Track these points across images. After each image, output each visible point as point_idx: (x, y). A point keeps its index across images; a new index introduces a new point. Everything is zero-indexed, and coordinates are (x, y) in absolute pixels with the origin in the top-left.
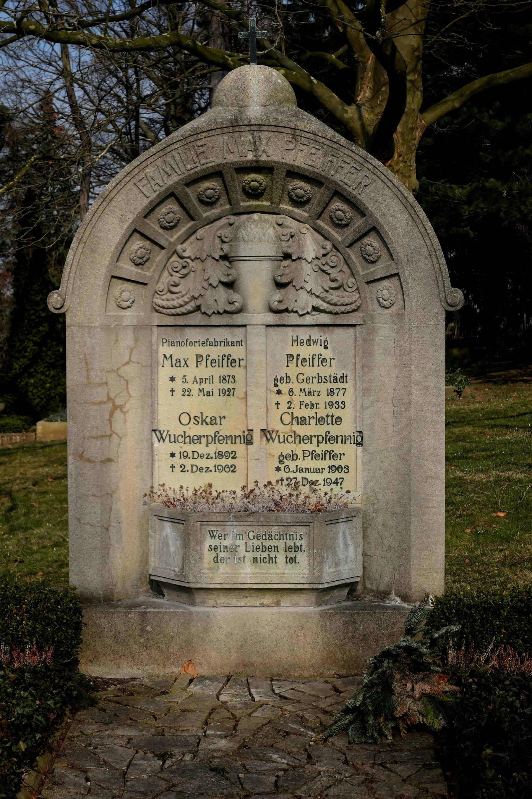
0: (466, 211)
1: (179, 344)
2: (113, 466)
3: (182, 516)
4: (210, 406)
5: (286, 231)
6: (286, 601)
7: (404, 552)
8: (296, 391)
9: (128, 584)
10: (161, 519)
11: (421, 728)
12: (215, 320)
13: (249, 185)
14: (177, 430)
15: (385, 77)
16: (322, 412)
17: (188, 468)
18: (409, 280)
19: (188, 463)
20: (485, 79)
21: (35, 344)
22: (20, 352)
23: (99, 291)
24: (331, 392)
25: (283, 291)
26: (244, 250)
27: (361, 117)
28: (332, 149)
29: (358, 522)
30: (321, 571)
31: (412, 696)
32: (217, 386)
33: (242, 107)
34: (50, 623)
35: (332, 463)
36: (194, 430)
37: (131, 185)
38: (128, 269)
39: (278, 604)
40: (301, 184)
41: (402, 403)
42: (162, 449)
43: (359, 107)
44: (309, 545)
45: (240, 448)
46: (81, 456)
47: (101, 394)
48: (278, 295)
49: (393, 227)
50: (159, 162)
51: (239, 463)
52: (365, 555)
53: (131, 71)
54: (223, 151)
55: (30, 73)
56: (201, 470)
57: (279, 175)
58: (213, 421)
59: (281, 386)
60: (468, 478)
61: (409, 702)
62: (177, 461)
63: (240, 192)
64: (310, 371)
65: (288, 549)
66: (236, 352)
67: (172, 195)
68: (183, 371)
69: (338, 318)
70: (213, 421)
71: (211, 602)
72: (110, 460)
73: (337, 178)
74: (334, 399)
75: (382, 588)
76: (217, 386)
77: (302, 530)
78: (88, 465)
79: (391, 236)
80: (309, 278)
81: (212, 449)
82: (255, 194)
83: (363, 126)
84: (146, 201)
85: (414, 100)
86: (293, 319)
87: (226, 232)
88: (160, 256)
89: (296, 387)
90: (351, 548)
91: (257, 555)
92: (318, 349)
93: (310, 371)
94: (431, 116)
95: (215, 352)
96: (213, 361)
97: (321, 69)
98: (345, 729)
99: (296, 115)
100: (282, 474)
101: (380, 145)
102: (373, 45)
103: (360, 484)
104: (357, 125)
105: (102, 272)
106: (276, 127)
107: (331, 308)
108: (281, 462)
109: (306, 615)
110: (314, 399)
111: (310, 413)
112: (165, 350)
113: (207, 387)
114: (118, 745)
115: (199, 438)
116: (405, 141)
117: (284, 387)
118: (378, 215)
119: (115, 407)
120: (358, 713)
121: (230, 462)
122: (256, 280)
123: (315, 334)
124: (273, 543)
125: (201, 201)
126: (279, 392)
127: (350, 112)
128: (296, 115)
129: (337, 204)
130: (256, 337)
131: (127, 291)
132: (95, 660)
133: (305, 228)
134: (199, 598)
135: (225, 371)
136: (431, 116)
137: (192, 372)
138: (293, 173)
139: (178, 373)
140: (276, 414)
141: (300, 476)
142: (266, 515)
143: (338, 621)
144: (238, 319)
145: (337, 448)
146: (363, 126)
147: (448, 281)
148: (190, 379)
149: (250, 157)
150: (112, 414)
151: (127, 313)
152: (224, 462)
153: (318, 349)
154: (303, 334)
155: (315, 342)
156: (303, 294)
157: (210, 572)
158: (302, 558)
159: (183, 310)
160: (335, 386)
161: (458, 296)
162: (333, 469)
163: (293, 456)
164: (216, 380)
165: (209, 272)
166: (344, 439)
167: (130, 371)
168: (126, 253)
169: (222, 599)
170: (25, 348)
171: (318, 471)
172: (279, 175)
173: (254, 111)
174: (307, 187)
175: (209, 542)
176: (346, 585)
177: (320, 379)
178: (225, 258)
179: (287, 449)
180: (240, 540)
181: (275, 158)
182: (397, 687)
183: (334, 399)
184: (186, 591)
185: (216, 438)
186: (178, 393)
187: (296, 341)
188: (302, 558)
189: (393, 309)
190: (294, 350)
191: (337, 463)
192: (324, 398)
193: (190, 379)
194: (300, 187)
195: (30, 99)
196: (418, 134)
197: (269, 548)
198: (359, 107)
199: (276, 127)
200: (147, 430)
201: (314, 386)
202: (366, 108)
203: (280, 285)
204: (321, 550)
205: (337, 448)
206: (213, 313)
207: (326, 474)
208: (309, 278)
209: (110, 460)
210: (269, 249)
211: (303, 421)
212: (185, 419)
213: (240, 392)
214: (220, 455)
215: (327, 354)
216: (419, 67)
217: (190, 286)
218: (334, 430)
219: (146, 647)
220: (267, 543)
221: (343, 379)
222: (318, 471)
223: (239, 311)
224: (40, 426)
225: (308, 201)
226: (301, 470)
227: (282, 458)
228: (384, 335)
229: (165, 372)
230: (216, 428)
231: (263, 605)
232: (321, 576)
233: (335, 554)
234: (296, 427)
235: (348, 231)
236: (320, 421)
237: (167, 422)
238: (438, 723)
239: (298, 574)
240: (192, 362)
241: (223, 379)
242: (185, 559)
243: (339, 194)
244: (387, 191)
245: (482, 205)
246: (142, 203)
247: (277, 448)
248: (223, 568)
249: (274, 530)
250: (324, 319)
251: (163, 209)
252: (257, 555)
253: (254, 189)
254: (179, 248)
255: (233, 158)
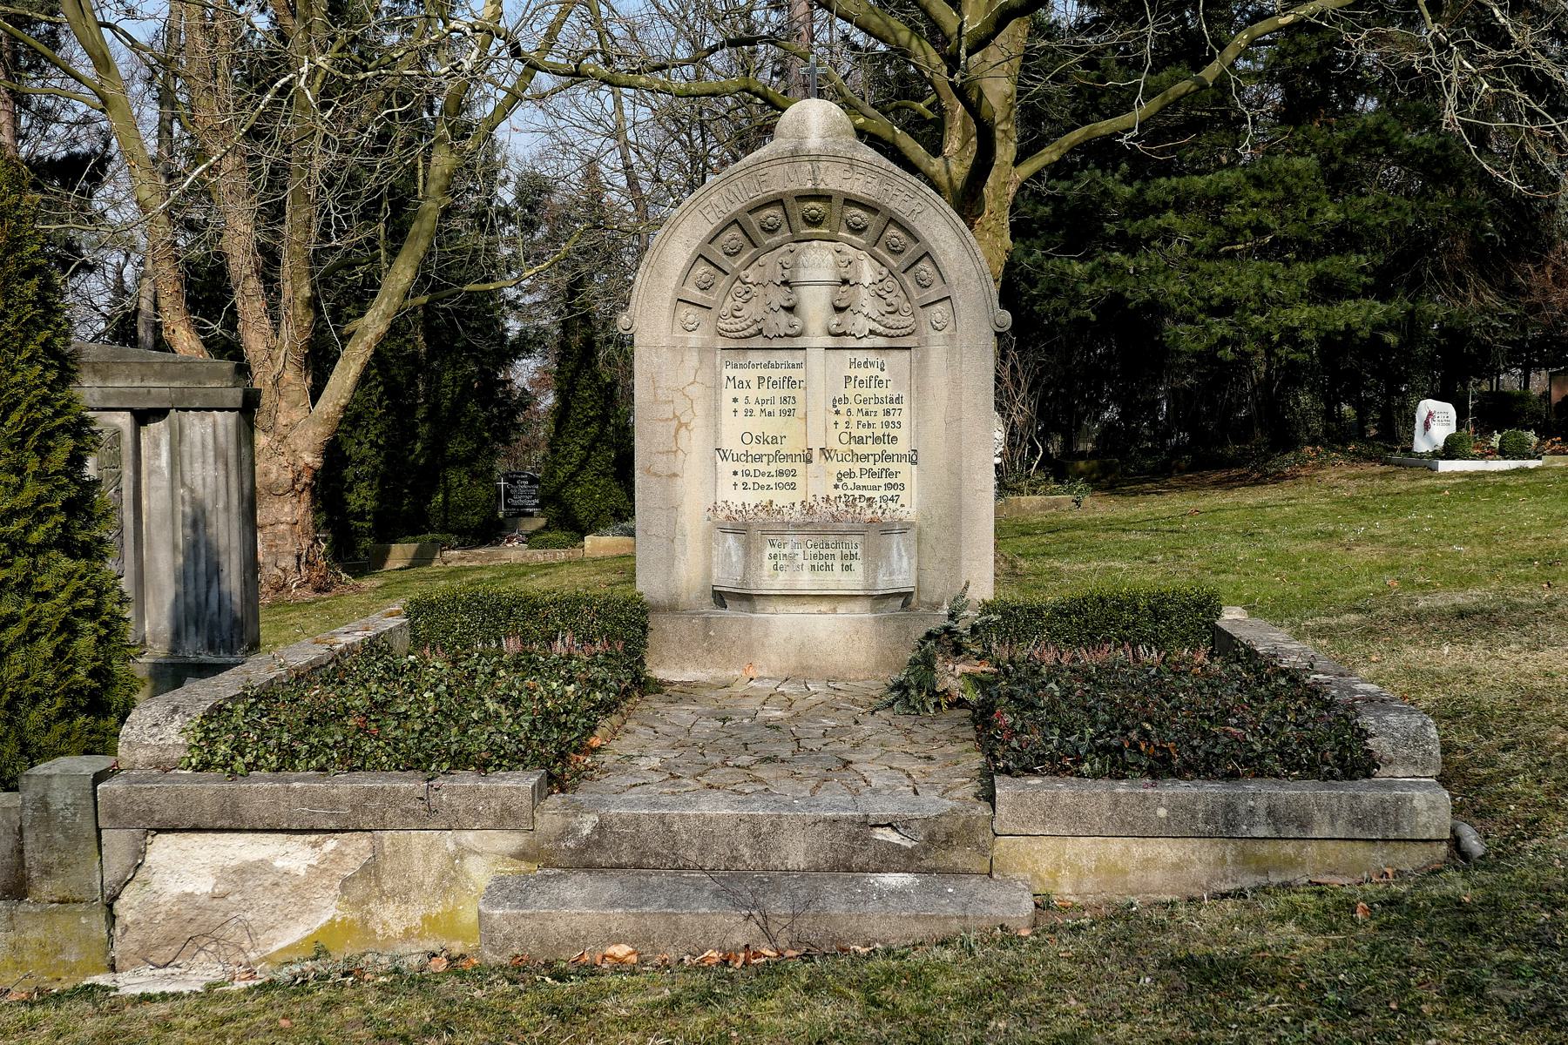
0: (1085, 289)
1: (742, 366)
2: (679, 481)
3: (744, 530)
4: (771, 426)
5: (844, 258)
6: (842, 608)
7: (955, 562)
8: (854, 411)
9: (693, 596)
10: (724, 531)
11: (960, 703)
12: (776, 343)
13: (809, 213)
14: (739, 449)
15: (973, 128)
16: (879, 432)
17: (750, 485)
18: (959, 302)
19: (750, 480)
20: (1086, 128)
21: (583, 448)
22: (564, 457)
23: (666, 313)
24: (887, 413)
25: (842, 315)
26: (804, 275)
27: (948, 171)
28: (886, 178)
29: (912, 534)
30: (875, 578)
31: (953, 676)
32: (777, 407)
33: (802, 139)
34: (619, 622)
35: (889, 480)
36: (756, 449)
37: (696, 212)
38: (694, 293)
39: (834, 611)
40: (859, 211)
41: (953, 420)
42: (726, 467)
43: (946, 159)
44: (864, 553)
45: (799, 466)
46: (648, 470)
47: (667, 411)
48: (836, 319)
49: (944, 253)
50: (723, 191)
51: (798, 480)
52: (919, 569)
53: (695, 134)
54: (782, 181)
55: (574, 135)
56: (762, 487)
57: (837, 203)
58: (775, 440)
59: (839, 407)
60: (1066, 568)
61: (950, 679)
62: (740, 479)
63: (800, 219)
64: (867, 392)
65: (844, 557)
66: (797, 374)
67: (736, 221)
68: (746, 392)
69: (894, 341)
70: (775, 440)
71: (771, 609)
72: (675, 475)
73: (892, 205)
74: (890, 419)
75: (935, 600)
76: (777, 407)
77: (857, 539)
78: (654, 479)
79: (942, 260)
80: (867, 302)
81: (773, 467)
82: (814, 222)
83: (950, 180)
84: (711, 227)
85: (1005, 152)
86: (850, 342)
87: (788, 259)
88: (723, 282)
89: (854, 408)
90: (905, 559)
91: (815, 563)
92: (875, 371)
93: (867, 392)
94: (1027, 169)
95: (776, 374)
96: (774, 383)
97: (900, 113)
98: (891, 705)
99: (854, 146)
100: (840, 492)
101: (968, 201)
102: (961, 92)
103: (915, 500)
104: (944, 180)
105: (669, 295)
106: (835, 157)
107: (887, 331)
108: (839, 479)
109: (861, 621)
110: (871, 419)
111: (868, 432)
112: (729, 372)
113: (768, 408)
114: (684, 715)
115: (761, 456)
116: (996, 197)
117: (842, 408)
118: (930, 240)
119: (681, 425)
120: (901, 687)
121: (790, 480)
122: (815, 303)
123: (872, 356)
124: (829, 552)
125: (763, 229)
126: (837, 412)
127: (936, 165)
128: (854, 146)
129: (893, 231)
130: (816, 358)
131: (691, 314)
132: (661, 663)
133: (862, 255)
134: (759, 605)
135: (786, 392)
136: (1027, 169)
137: (754, 392)
138: (850, 201)
139: (741, 394)
140: (834, 433)
141: (857, 493)
142: (824, 529)
143: (892, 626)
144: (799, 342)
145: (893, 466)
146: (950, 180)
147: (997, 304)
148: (752, 400)
149: (809, 185)
150: (677, 431)
151: (692, 335)
152: (784, 480)
153: (875, 371)
154: (861, 356)
155: (872, 364)
156: (860, 319)
157: (769, 579)
158: (857, 565)
159: (746, 333)
160: (891, 406)
161: (1006, 317)
162: (889, 486)
163: (850, 474)
164: (777, 401)
165: (771, 297)
166: (900, 458)
167: (695, 391)
168: (691, 277)
169: (781, 607)
170: (570, 453)
171: (875, 488)
172: (837, 203)
173: (814, 142)
174: (864, 214)
175: (769, 550)
176: (900, 595)
177: (878, 401)
178: (785, 283)
179: (845, 467)
180: (799, 549)
181: (832, 186)
182: (938, 666)
183: (890, 419)
184: (747, 598)
185: (778, 457)
186: (741, 413)
187: (854, 364)
188: (857, 565)
189: (945, 331)
190: (852, 372)
191: (893, 481)
192: (881, 418)
193: (752, 400)
194: (856, 214)
195: (572, 167)
196: (1012, 189)
197: (826, 557)
198: (946, 159)
199: (835, 157)
200: (711, 449)
201: (871, 407)
202: (956, 159)
203: (839, 310)
204: (876, 557)
205: (893, 466)
206: (771, 336)
207: (882, 492)
208: (867, 302)
209: (675, 475)
210: (827, 274)
211: (860, 441)
212: (747, 438)
213: (800, 412)
214: (781, 473)
215: (883, 376)
216: (1013, 115)
217: (752, 310)
218: (890, 449)
219: (709, 651)
220: (824, 552)
221: (899, 399)
222: (875, 488)
223: (799, 335)
224: (589, 540)
225: (865, 228)
226: (858, 488)
227: (840, 476)
228: (937, 355)
229: (729, 393)
230: (777, 447)
231: (820, 613)
232: (875, 583)
233: (889, 564)
234: (853, 446)
235: (903, 257)
236: (876, 440)
237: (731, 443)
238: (973, 696)
239: (853, 580)
240: (754, 384)
241: (784, 400)
242: (746, 567)
243: (893, 221)
244: (939, 218)
245: (1105, 284)
246: (706, 229)
247: (836, 467)
248: (782, 576)
249: (831, 539)
250: (880, 342)
251: (727, 236)
252: (815, 563)
253: (814, 217)
254: (742, 274)
255: (793, 186)
